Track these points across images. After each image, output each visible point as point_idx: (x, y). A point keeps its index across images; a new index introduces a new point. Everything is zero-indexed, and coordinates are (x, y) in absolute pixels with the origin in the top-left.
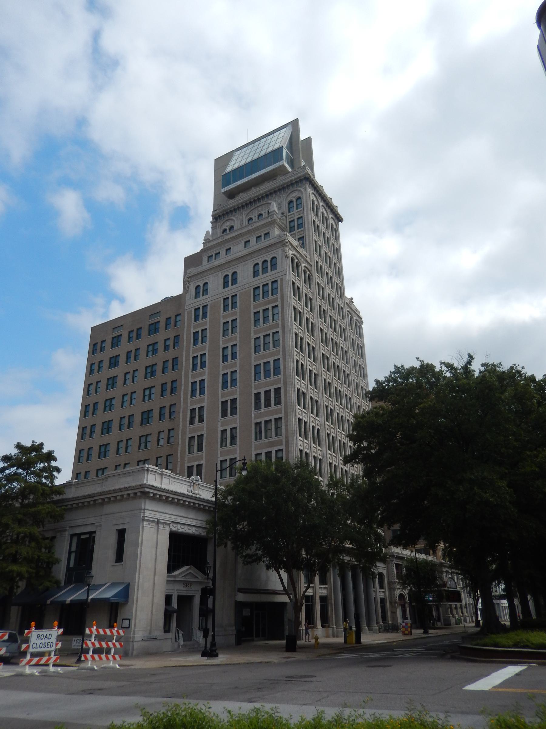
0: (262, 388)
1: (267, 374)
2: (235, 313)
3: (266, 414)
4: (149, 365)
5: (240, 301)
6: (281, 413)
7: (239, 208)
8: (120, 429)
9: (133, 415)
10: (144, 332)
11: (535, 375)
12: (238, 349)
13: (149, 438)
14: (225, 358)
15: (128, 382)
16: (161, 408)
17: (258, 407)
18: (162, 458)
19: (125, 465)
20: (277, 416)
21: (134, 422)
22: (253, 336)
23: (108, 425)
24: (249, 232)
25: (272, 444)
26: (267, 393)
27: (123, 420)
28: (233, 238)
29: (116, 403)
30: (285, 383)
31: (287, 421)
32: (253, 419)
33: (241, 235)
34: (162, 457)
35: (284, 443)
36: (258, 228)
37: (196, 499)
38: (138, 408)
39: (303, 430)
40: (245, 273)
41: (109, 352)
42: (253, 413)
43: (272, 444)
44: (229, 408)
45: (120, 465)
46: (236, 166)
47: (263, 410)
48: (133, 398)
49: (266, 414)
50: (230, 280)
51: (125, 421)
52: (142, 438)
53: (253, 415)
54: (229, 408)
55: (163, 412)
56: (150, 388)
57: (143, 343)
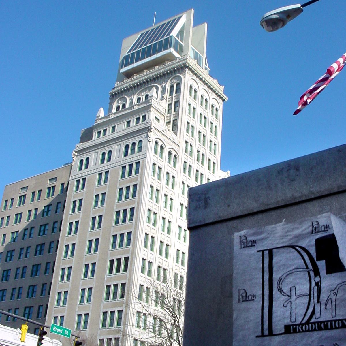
0: (108, 308)
3: (117, 279)
4: (39, 243)
5: (110, 177)
6: (129, 253)
7: (118, 93)
8: (15, 278)
9: (26, 267)
11: (285, 325)
13: (47, 227)
15: (26, 237)
16: (43, 284)
19: (16, 309)
21: (26, 274)
23: (7, 273)
27: (19, 270)
31: (126, 314)
32: (105, 281)
34: (42, 306)
35: (131, 252)
41: (17, 208)
45: (11, 309)
48: (32, 232)
51: (20, 272)
52: (30, 287)
53: (106, 279)
55: (44, 288)
56: (45, 225)
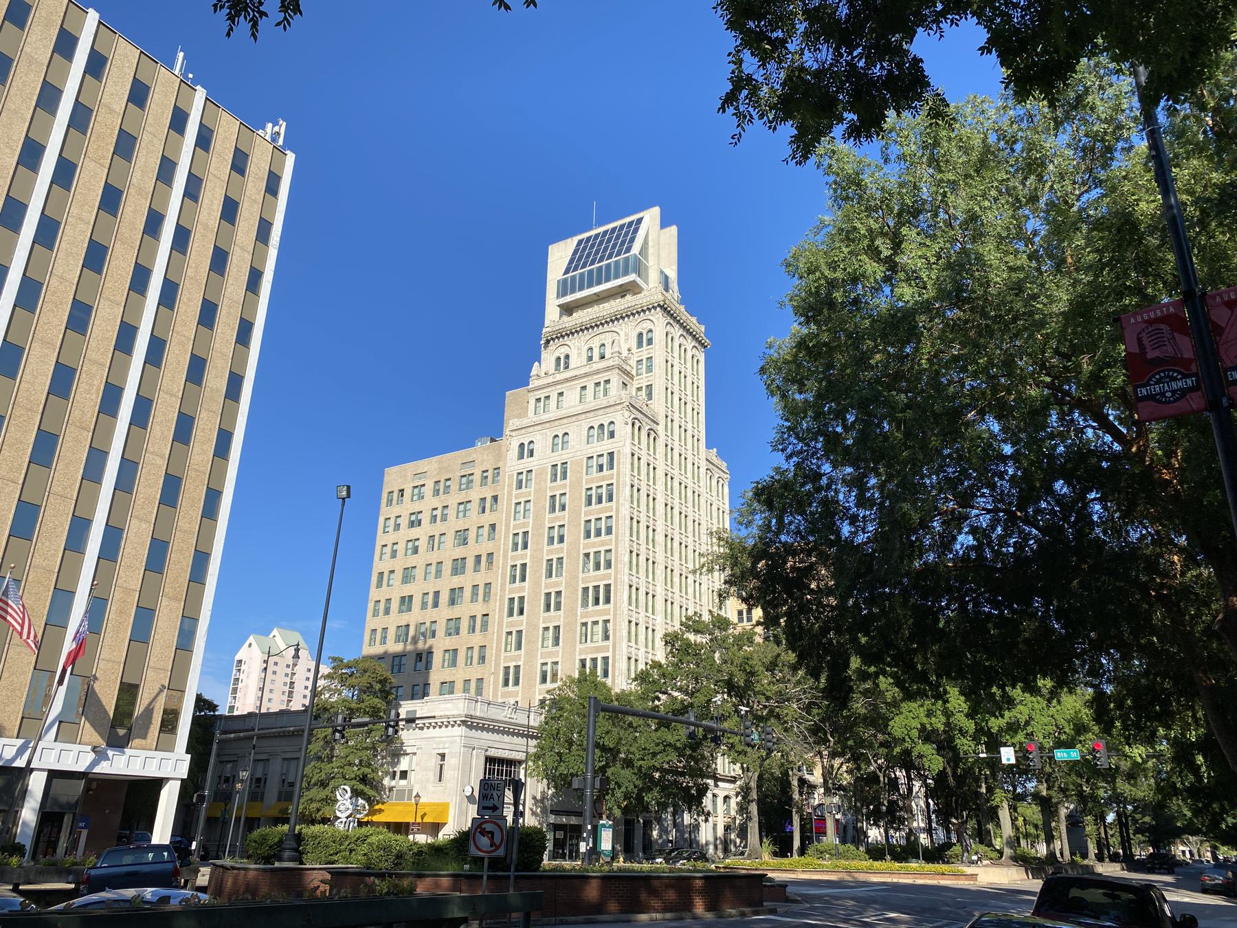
1: (597, 567)
2: (564, 486)
3: (596, 544)
10: (454, 486)
12: (566, 531)
14: (551, 540)
17: (585, 604)
18: (432, 775)
20: (606, 618)
22: (584, 518)
24: (586, 375)
25: (598, 650)
26: (596, 588)
28: (567, 380)
29: (419, 573)
30: (616, 579)
33: (575, 378)
36: (598, 372)
37: (510, 724)
38: (446, 584)
39: (633, 634)
40: (577, 433)
42: (580, 610)
43: (598, 650)
44: (552, 602)
46: (675, 267)
47: (591, 608)
49: (596, 544)
50: (559, 441)
54: (552, 602)
57: (453, 500)
